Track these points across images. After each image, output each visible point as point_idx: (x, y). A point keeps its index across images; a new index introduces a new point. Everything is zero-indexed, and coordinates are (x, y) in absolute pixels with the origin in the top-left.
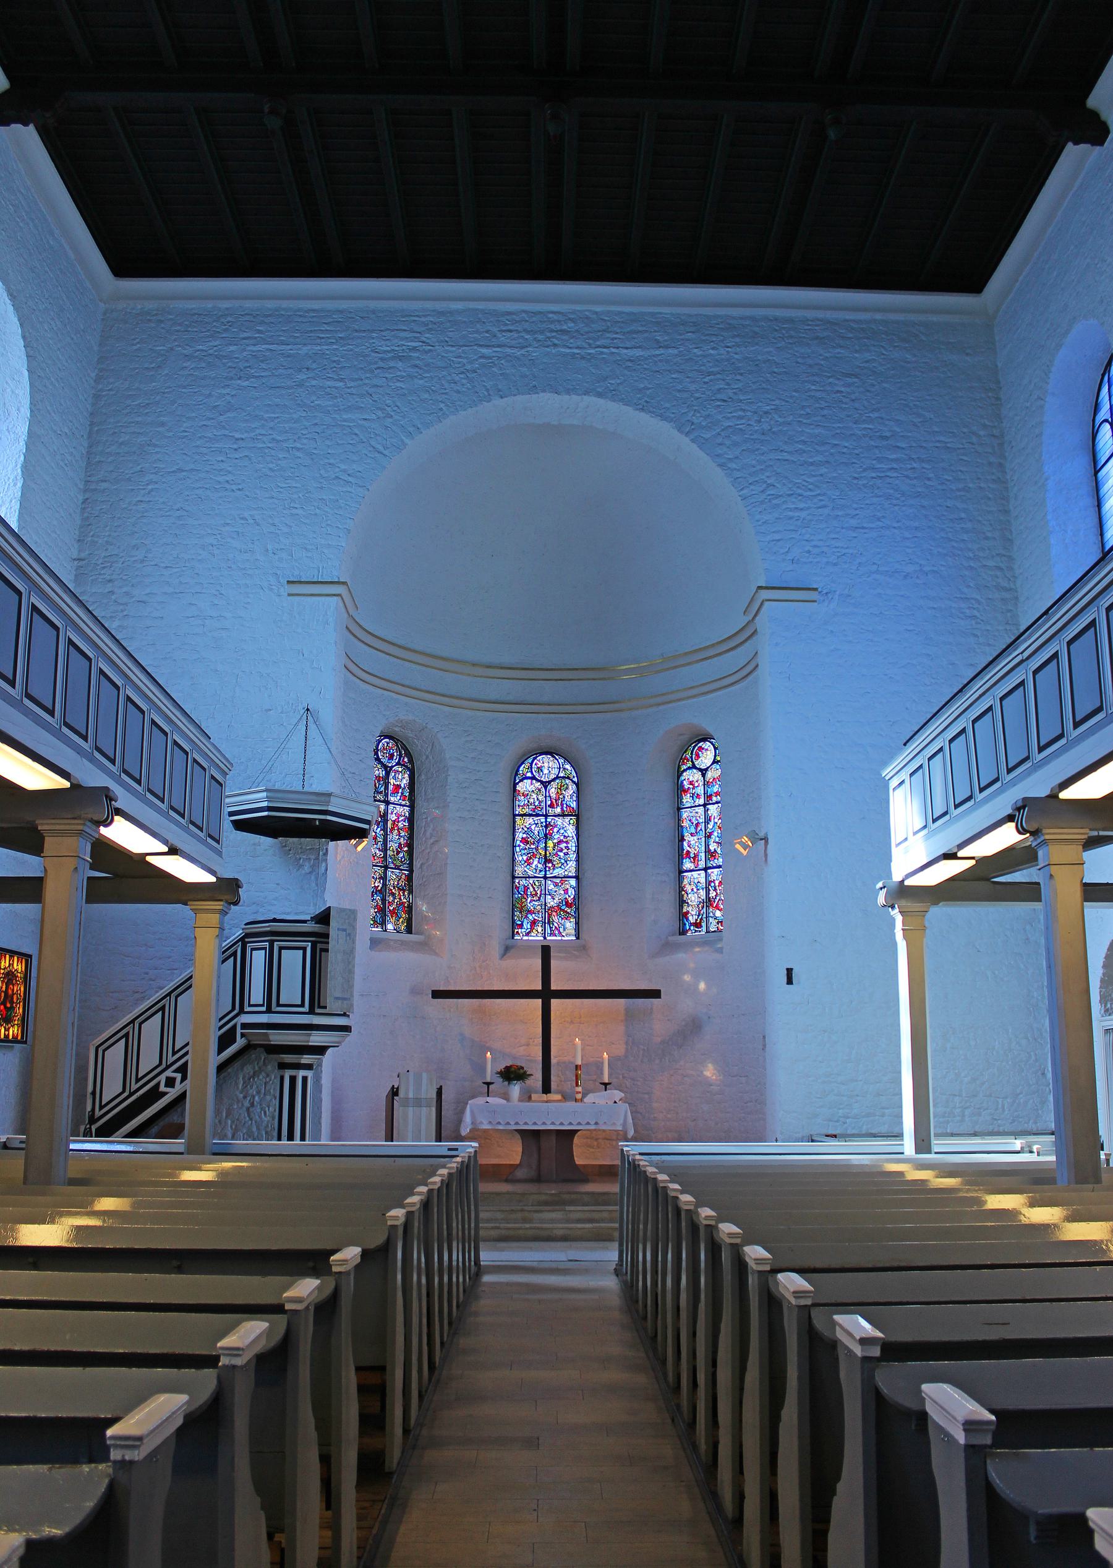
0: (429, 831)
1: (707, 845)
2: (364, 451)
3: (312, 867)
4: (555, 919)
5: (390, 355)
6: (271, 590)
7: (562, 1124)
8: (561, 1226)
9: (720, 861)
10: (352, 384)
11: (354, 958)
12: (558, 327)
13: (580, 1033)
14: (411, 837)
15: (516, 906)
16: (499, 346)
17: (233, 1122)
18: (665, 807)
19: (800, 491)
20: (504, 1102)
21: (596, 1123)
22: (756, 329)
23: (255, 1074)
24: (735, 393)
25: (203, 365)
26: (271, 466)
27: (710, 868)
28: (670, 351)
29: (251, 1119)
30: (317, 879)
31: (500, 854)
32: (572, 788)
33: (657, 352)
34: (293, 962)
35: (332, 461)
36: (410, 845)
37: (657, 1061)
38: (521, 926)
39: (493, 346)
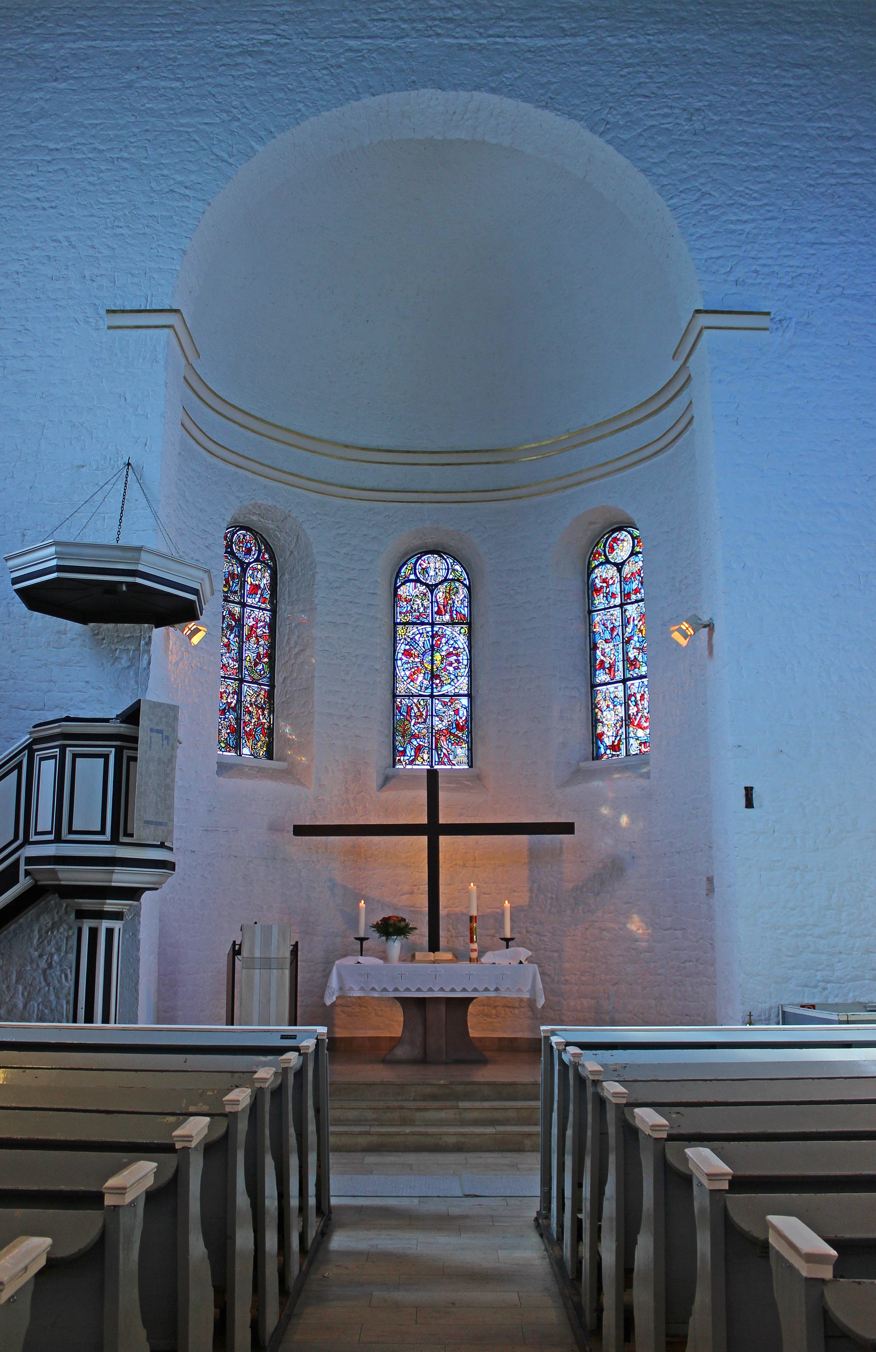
0: (294, 638)
1: (625, 653)
2: (205, 160)
3: (131, 660)
4: (444, 744)
5: (237, 50)
6: (88, 323)
7: (453, 990)
8: (452, 1130)
9: (644, 670)
10: (191, 84)
11: (173, 769)
12: (442, 15)
13: (476, 876)
14: (272, 646)
15: (398, 729)
16: (369, 37)
17: (25, 988)
18: (576, 610)
19: (742, 201)
20: (382, 962)
21: (497, 989)
22: (684, 14)
23: (55, 926)
24: (659, 88)
25: (12, 66)
26: (91, 179)
27: (629, 679)
28: (579, 40)
29: (48, 985)
30: (136, 674)
31: (378, 667)
32: (463, 592)
33: (563, 42)
34: (90, 774)
35: (165, 172)
36: (271, 655)
37: (568, 912)
38: (404, 753)
39: (363, 38)
